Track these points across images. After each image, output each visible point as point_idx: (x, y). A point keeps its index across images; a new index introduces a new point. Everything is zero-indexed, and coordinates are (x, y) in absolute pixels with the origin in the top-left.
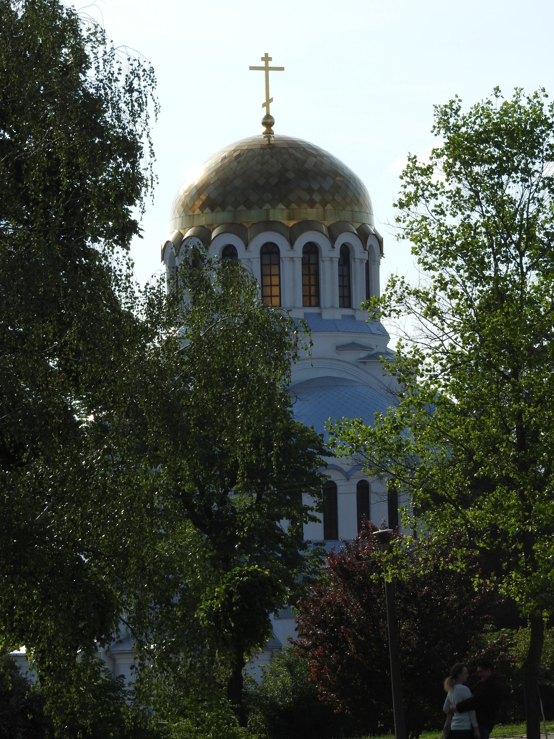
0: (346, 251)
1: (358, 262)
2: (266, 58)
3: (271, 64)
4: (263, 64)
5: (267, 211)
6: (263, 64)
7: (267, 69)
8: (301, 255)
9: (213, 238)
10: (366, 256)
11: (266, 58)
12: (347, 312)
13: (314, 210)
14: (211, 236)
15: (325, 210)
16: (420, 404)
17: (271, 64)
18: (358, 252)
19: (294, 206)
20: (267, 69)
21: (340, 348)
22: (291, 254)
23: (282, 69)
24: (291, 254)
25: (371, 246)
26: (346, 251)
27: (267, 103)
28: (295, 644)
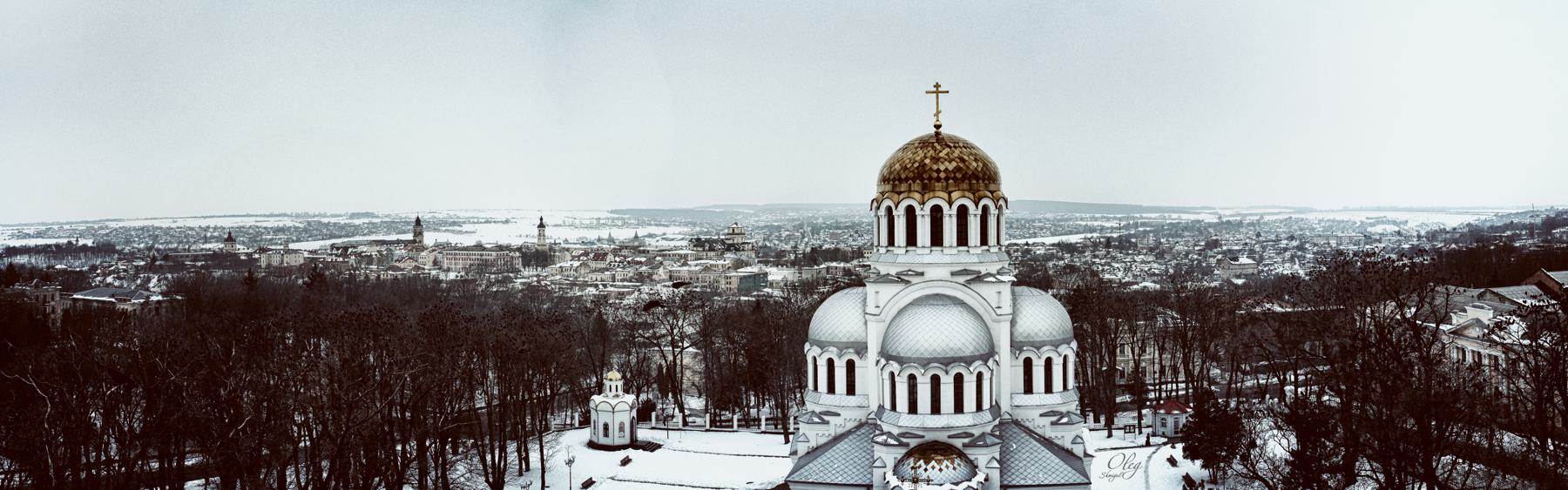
0: (985, 209)
1: (972, 216)
2: (937, 86)
3: (940, 89)
4: (935, 89)
5: (910, 184)
6: (935, 89)
7: (937, 92)
8: (929, 213)
9: (1495, 290)
10: (997, 212)
11: (937, 86)
12: (985, 248)
13: (940, 184)
14: (1493, 287)
15: (947, 184)
16: (321, 302)
17: (940, 89)
18: (993, 210)
19: (986, 182)
20: (937, 92)
21: (953, 274)
22: (922, 213)
23: (948, 92)
24: (922, 213)
25: (1001, 205)
26: (985, 209)
27: (938, 113)
28: (1539, 247)
